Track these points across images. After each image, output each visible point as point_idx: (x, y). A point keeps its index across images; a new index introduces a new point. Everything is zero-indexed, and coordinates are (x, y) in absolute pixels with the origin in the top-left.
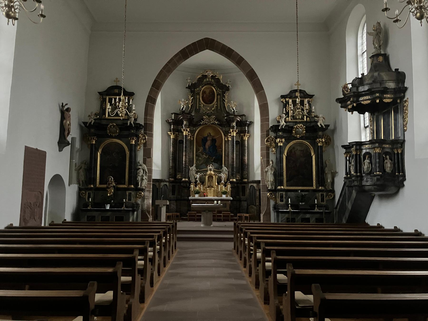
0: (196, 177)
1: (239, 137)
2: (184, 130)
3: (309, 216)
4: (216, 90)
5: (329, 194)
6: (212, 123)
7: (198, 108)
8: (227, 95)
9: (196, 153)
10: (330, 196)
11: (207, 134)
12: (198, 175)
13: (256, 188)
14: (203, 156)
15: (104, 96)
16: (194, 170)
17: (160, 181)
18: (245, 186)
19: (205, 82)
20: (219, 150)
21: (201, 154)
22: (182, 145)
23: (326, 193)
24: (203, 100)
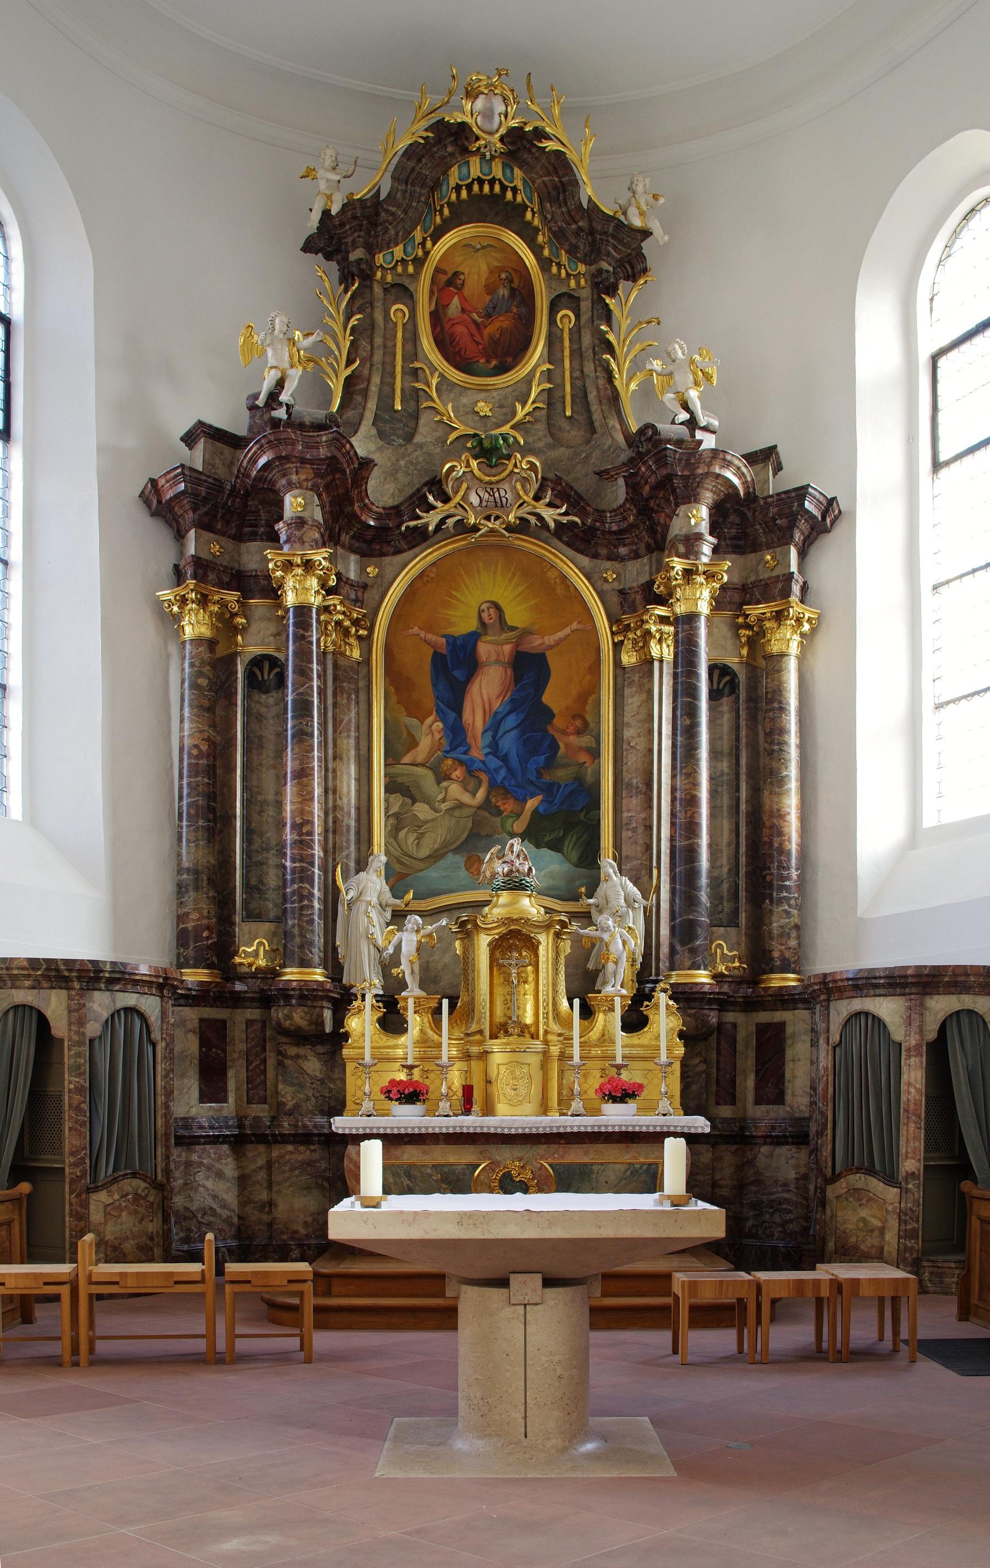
1: (729, 635)
2: (288, 566)
4: (544, 264)
6: (511, 518)
7: (398, 407)
8: (625, 313)
9: (393, 770)
11: (475, 616)
13: (898, 1033)
14: (446, 789)
16: (375, 900)
17: (79, 979)
18: (781, 1026)
19: (458, 188)
20: (573, 739)
21: (426, 777)
22: (270, 699)
24: (441, 343)
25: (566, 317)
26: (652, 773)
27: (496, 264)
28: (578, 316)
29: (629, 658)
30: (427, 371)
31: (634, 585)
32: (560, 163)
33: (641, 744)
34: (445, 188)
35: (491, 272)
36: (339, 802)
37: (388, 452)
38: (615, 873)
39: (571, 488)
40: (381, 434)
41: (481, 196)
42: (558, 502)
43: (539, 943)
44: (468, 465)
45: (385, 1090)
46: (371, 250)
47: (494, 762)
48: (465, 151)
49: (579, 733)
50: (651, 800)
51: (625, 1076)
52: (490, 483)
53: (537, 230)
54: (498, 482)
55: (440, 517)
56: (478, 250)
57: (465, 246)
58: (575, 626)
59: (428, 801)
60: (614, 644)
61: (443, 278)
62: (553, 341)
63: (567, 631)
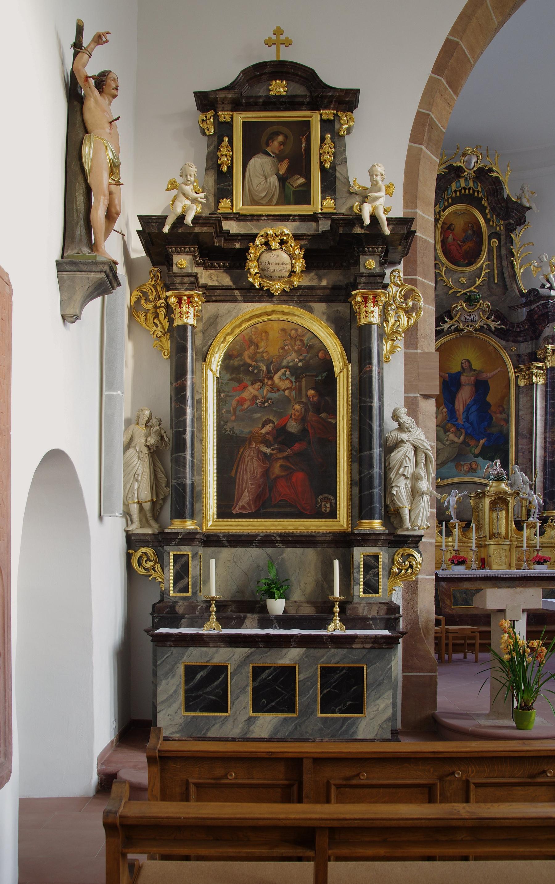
0: (446, 503)
4: (487, 221)
11: (460, 365)
12: (451, 498)
14: (448, 436)
15: (223, 111)
19: (455, 191)
20: (499, 415)
25: (495, 242)
26: (532, 430)
29: (522, 383)
30: (440, 265)
31: (524, 353)
33: (527, 418)
34: (450, 191)
35: (465, 224)
38: (518, 471)
39: (502, 314)
41: (465, 195)
42: (496, 320)
43: (509, 501)
44: (461, 305)
45: (451, 560)
47: (467, 425)
49: (501, 413)
50: (532, 441)
52: (470, 312)
53: (486, 208)
55: (450, 325)
56: (460, 215)
57: (454, 213)
58: (499, 369)
60: (515, 376)
61: (446, 226)
62: (490, 251)
63: (496, 371)
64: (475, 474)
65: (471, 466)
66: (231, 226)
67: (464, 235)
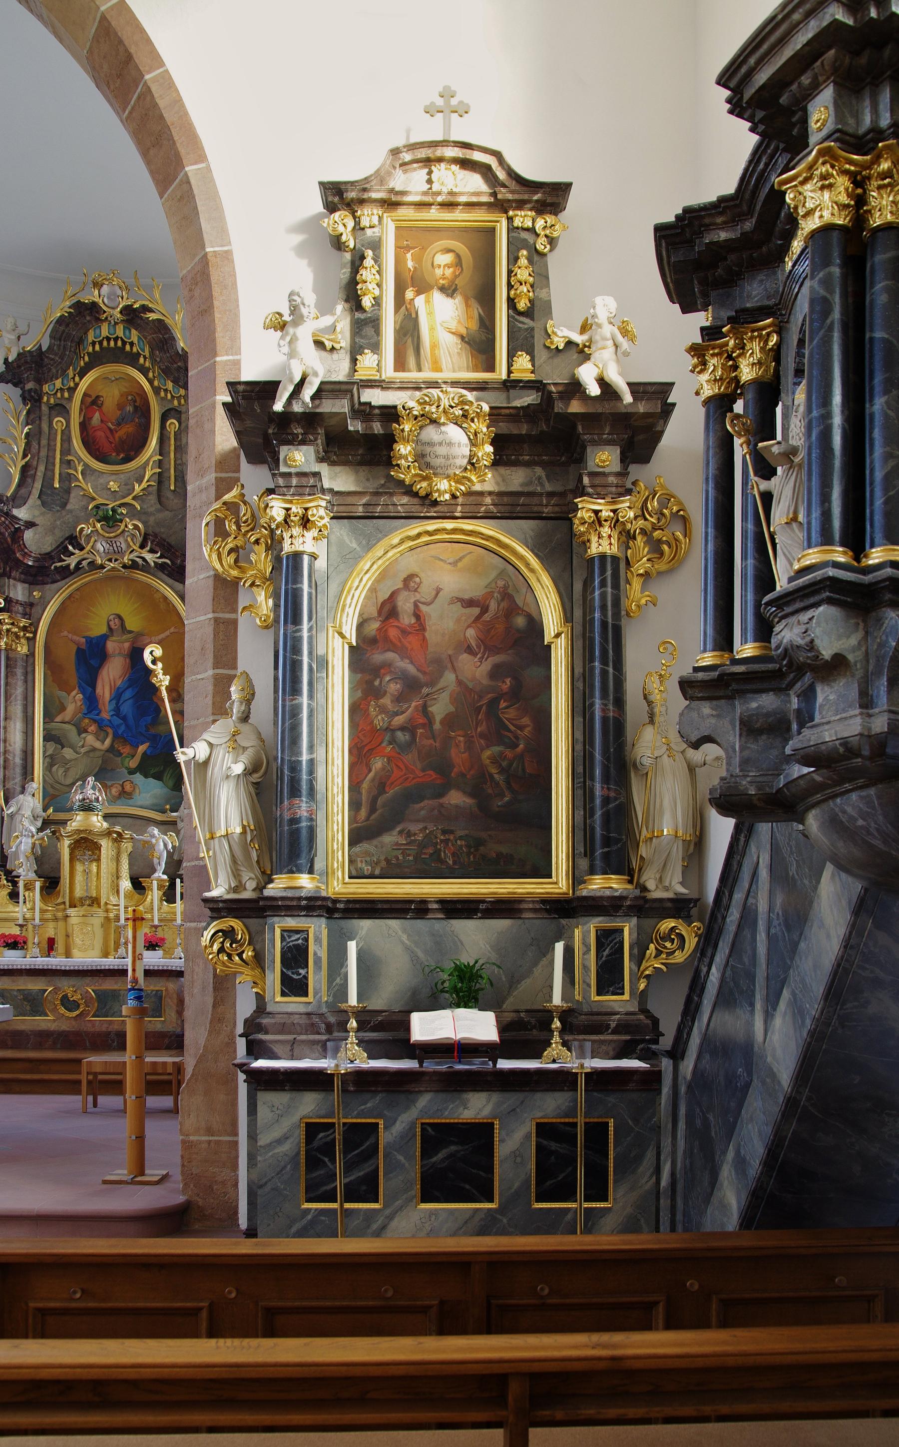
3: (486, 1112)
4: (157, 390)
5: (667, 924)
7: (57, 485)
9: (47, 726)
10: (668, 944)
14: (85, 738)
21: (72, 731)
23: (634, 920)
27: (125, 390)
28: (180, 424)
30: (76, 462)
32: (161, 326)
35: (122, 396)
36: (9, 748)
37: (49, 515)
40: (44, 504)
42: (157, 549)
44: (94, 527)
46: (40, 381)
47: (117, 721)
48: (98, 320)
51: (160, 934)
54: (115, 537)
57: (105, 378)
59: (72, 747)
61: (89, 400)
63: (167, 633)
64: (131, 802)
65: (123, 788)
66: (376, 397)
67: (119, 413)
